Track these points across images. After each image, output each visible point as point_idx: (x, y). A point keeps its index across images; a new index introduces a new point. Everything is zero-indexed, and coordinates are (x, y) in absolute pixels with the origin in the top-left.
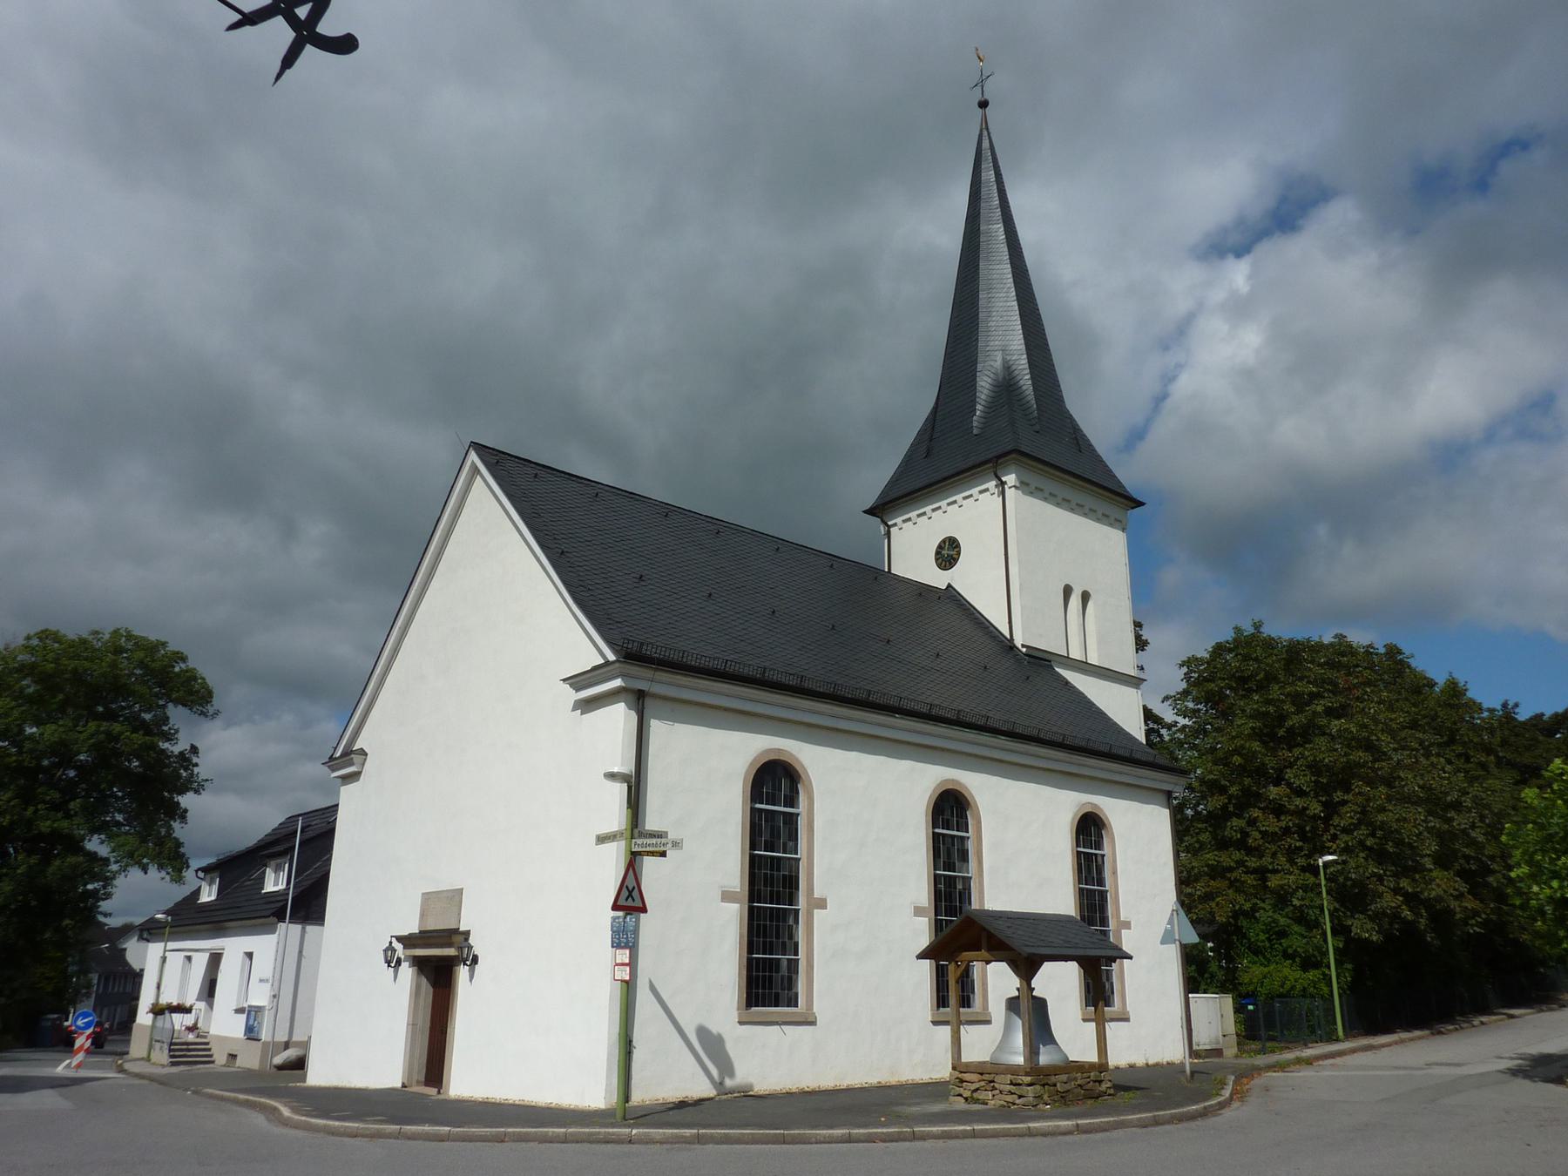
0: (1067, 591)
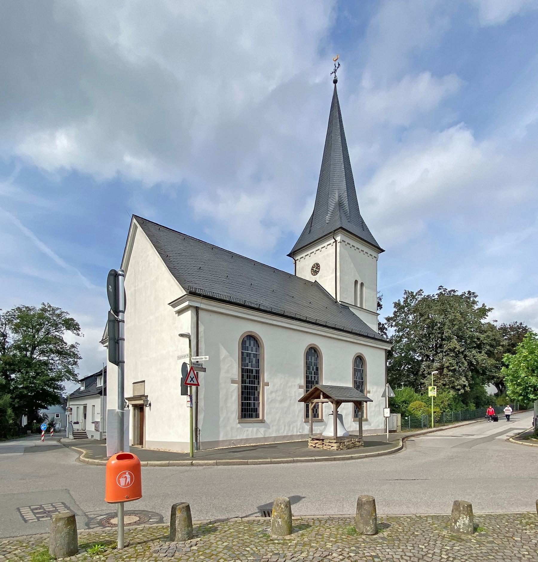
0: (356, 282)
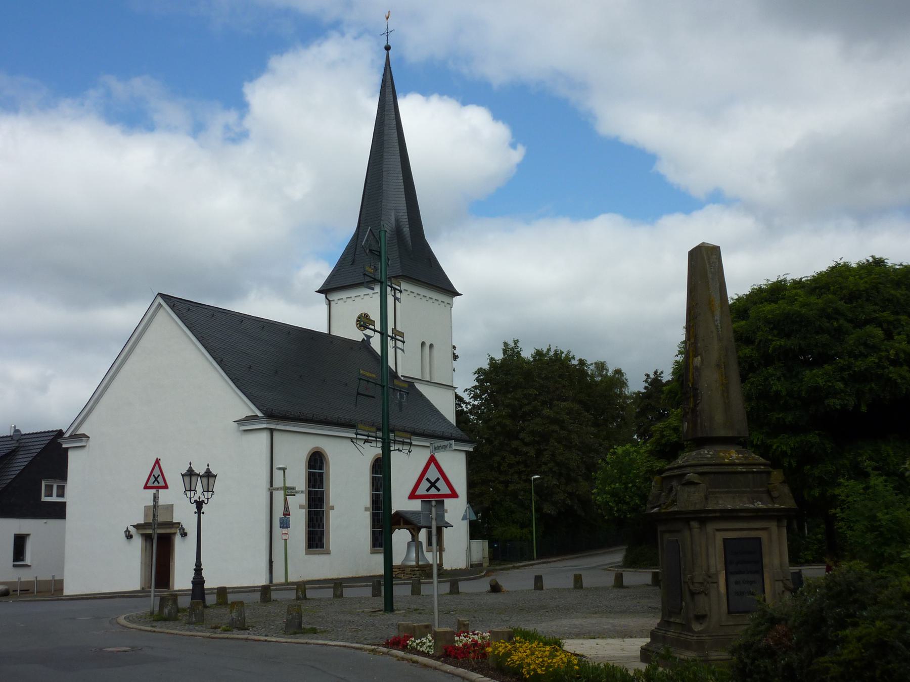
0: (423, 344)
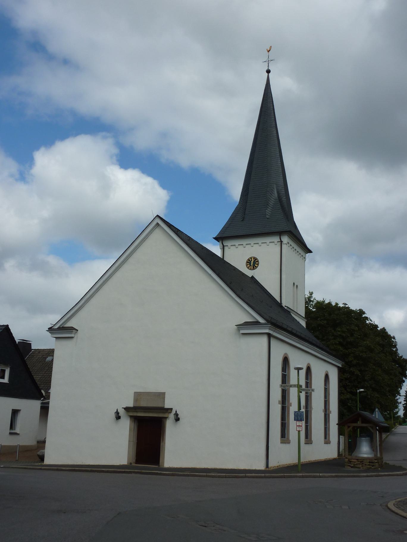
0: (294, 283)
